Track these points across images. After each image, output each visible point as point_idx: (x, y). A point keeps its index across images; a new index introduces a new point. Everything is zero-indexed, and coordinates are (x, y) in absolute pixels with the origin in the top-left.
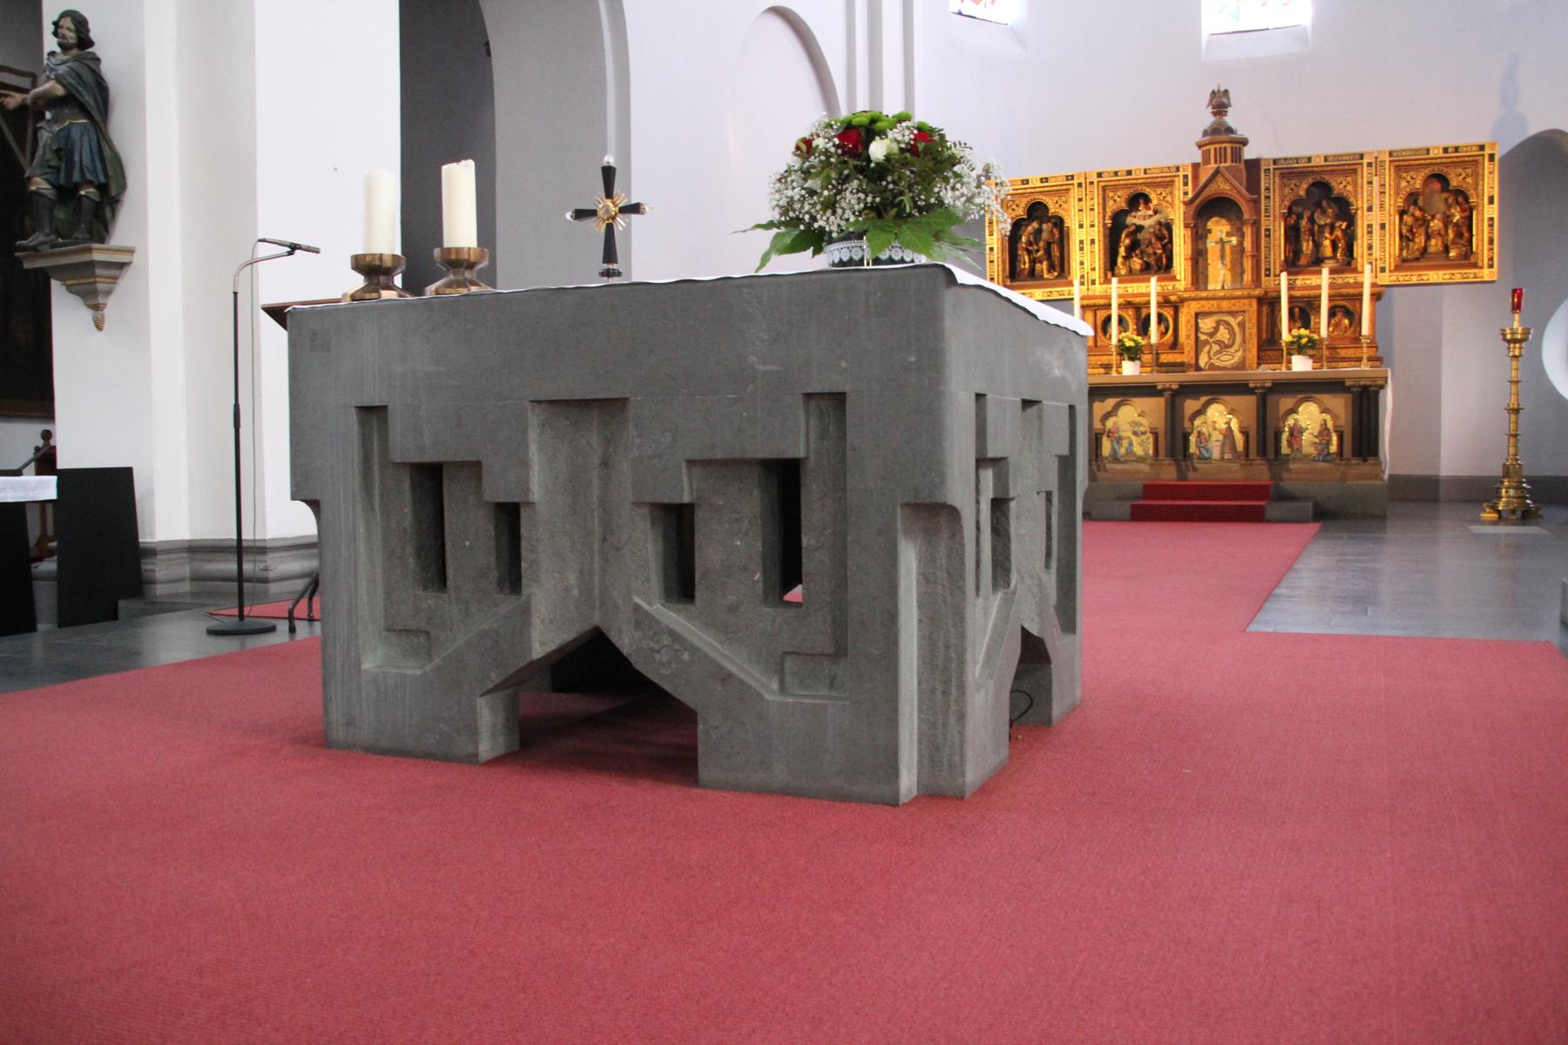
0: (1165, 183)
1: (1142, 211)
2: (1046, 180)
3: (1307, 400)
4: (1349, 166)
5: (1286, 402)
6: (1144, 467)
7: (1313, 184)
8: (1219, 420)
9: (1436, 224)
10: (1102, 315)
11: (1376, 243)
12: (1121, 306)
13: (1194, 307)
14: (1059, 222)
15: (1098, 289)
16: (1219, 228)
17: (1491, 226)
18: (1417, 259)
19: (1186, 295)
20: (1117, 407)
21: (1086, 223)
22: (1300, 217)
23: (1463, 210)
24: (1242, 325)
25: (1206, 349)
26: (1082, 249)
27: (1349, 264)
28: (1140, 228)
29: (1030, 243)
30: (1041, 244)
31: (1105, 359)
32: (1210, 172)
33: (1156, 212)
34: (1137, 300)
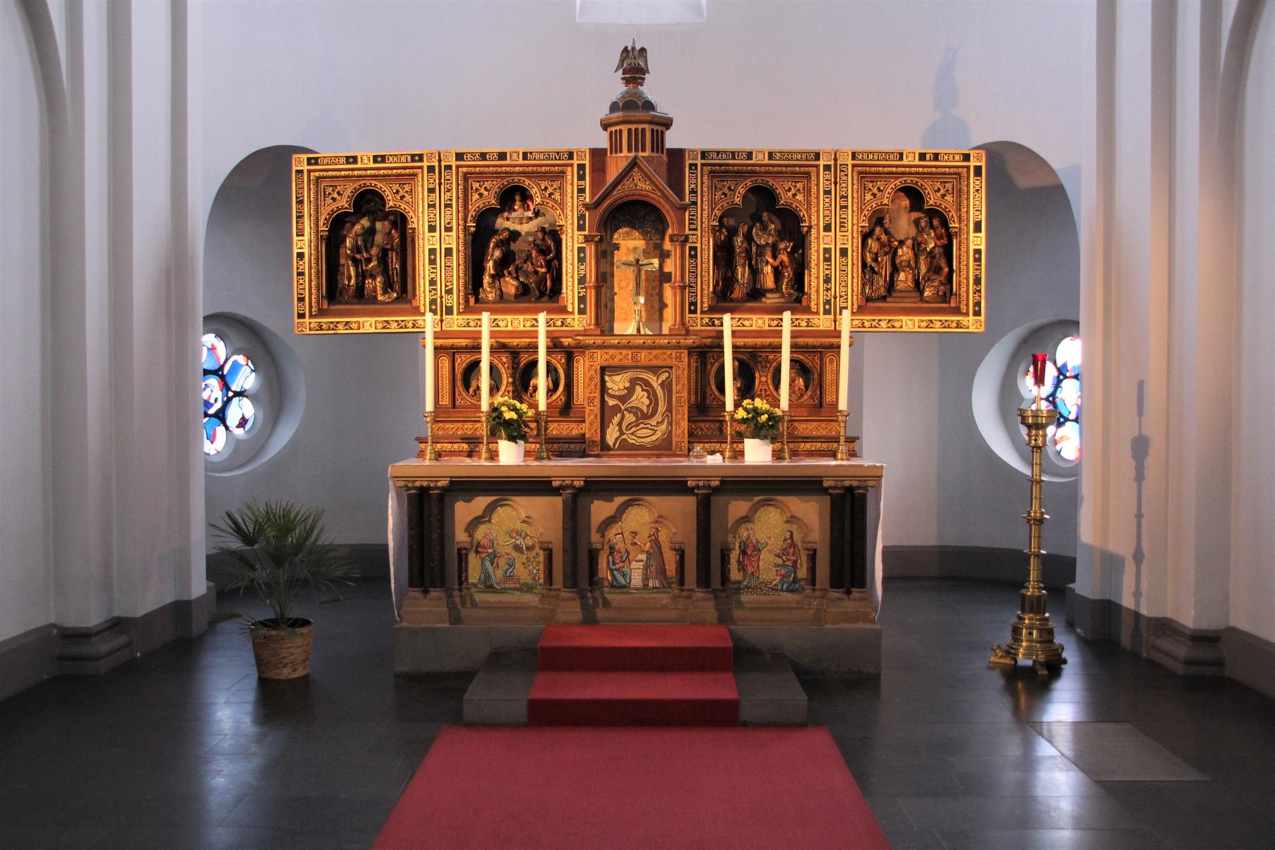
0: (552, 170)
1: (518, 211)
2: (383, 159)
3: (765, 503)
4: (801, 168)
5: (738, 507)
6: (531, 599)
7: (750, 190)
8: (640, 536)
9: (905, 253)
10: (462, 361)
11: (836, 275)
12: (494, 350)
13: (600, 358)
14: (400, 221)
15: (456, 322)
16: (629, 243)
17: (978, 260)
18: (884, 298)
19: (589, 341)
20: (490, 509)
21: (440, 223)
22: (733, 232)
23: (939, 237)
24: (667, 386)
25: (616, 419)
26: (432, 262)
27: (799, 300)
28: (514, 235)
29: (357, 249)
30: (374, 251)
31: (468, 429)
32: (623, 165)
33: (537, 214)
34: (515, 342)
